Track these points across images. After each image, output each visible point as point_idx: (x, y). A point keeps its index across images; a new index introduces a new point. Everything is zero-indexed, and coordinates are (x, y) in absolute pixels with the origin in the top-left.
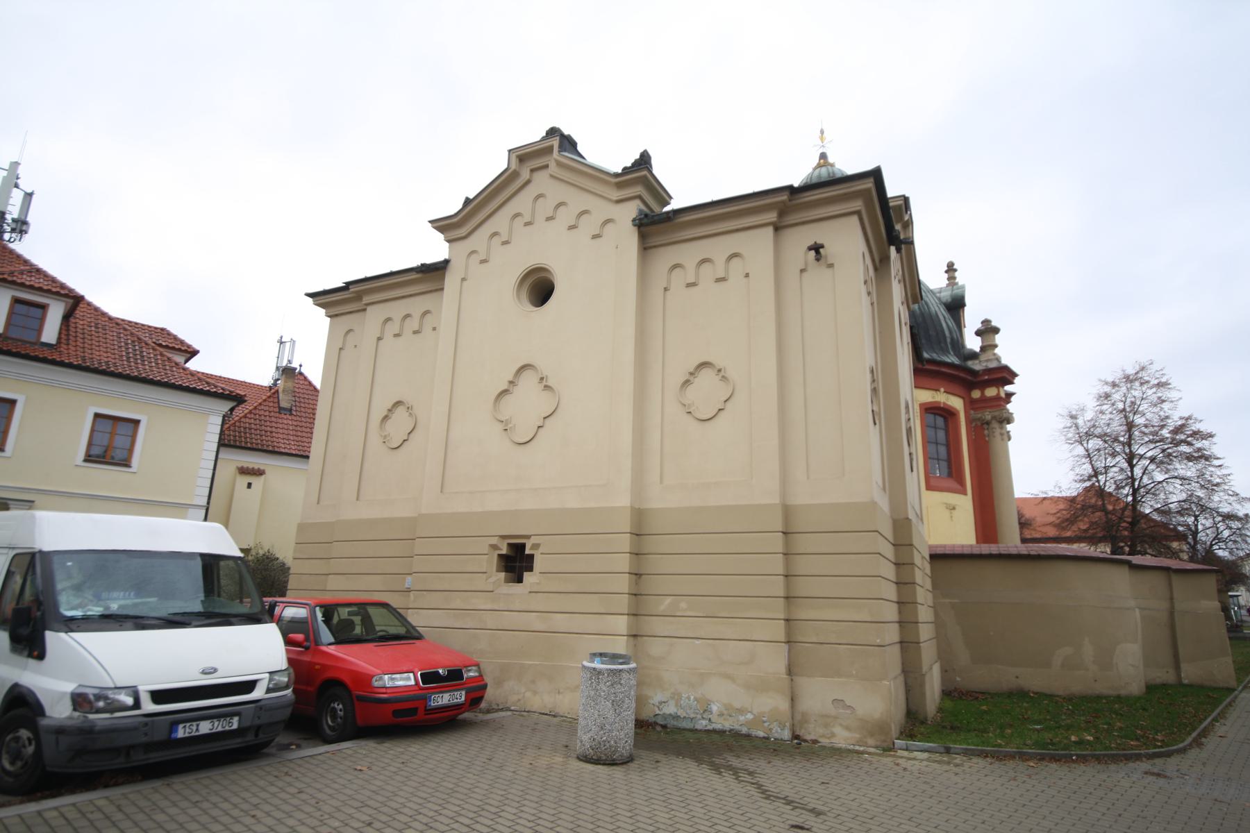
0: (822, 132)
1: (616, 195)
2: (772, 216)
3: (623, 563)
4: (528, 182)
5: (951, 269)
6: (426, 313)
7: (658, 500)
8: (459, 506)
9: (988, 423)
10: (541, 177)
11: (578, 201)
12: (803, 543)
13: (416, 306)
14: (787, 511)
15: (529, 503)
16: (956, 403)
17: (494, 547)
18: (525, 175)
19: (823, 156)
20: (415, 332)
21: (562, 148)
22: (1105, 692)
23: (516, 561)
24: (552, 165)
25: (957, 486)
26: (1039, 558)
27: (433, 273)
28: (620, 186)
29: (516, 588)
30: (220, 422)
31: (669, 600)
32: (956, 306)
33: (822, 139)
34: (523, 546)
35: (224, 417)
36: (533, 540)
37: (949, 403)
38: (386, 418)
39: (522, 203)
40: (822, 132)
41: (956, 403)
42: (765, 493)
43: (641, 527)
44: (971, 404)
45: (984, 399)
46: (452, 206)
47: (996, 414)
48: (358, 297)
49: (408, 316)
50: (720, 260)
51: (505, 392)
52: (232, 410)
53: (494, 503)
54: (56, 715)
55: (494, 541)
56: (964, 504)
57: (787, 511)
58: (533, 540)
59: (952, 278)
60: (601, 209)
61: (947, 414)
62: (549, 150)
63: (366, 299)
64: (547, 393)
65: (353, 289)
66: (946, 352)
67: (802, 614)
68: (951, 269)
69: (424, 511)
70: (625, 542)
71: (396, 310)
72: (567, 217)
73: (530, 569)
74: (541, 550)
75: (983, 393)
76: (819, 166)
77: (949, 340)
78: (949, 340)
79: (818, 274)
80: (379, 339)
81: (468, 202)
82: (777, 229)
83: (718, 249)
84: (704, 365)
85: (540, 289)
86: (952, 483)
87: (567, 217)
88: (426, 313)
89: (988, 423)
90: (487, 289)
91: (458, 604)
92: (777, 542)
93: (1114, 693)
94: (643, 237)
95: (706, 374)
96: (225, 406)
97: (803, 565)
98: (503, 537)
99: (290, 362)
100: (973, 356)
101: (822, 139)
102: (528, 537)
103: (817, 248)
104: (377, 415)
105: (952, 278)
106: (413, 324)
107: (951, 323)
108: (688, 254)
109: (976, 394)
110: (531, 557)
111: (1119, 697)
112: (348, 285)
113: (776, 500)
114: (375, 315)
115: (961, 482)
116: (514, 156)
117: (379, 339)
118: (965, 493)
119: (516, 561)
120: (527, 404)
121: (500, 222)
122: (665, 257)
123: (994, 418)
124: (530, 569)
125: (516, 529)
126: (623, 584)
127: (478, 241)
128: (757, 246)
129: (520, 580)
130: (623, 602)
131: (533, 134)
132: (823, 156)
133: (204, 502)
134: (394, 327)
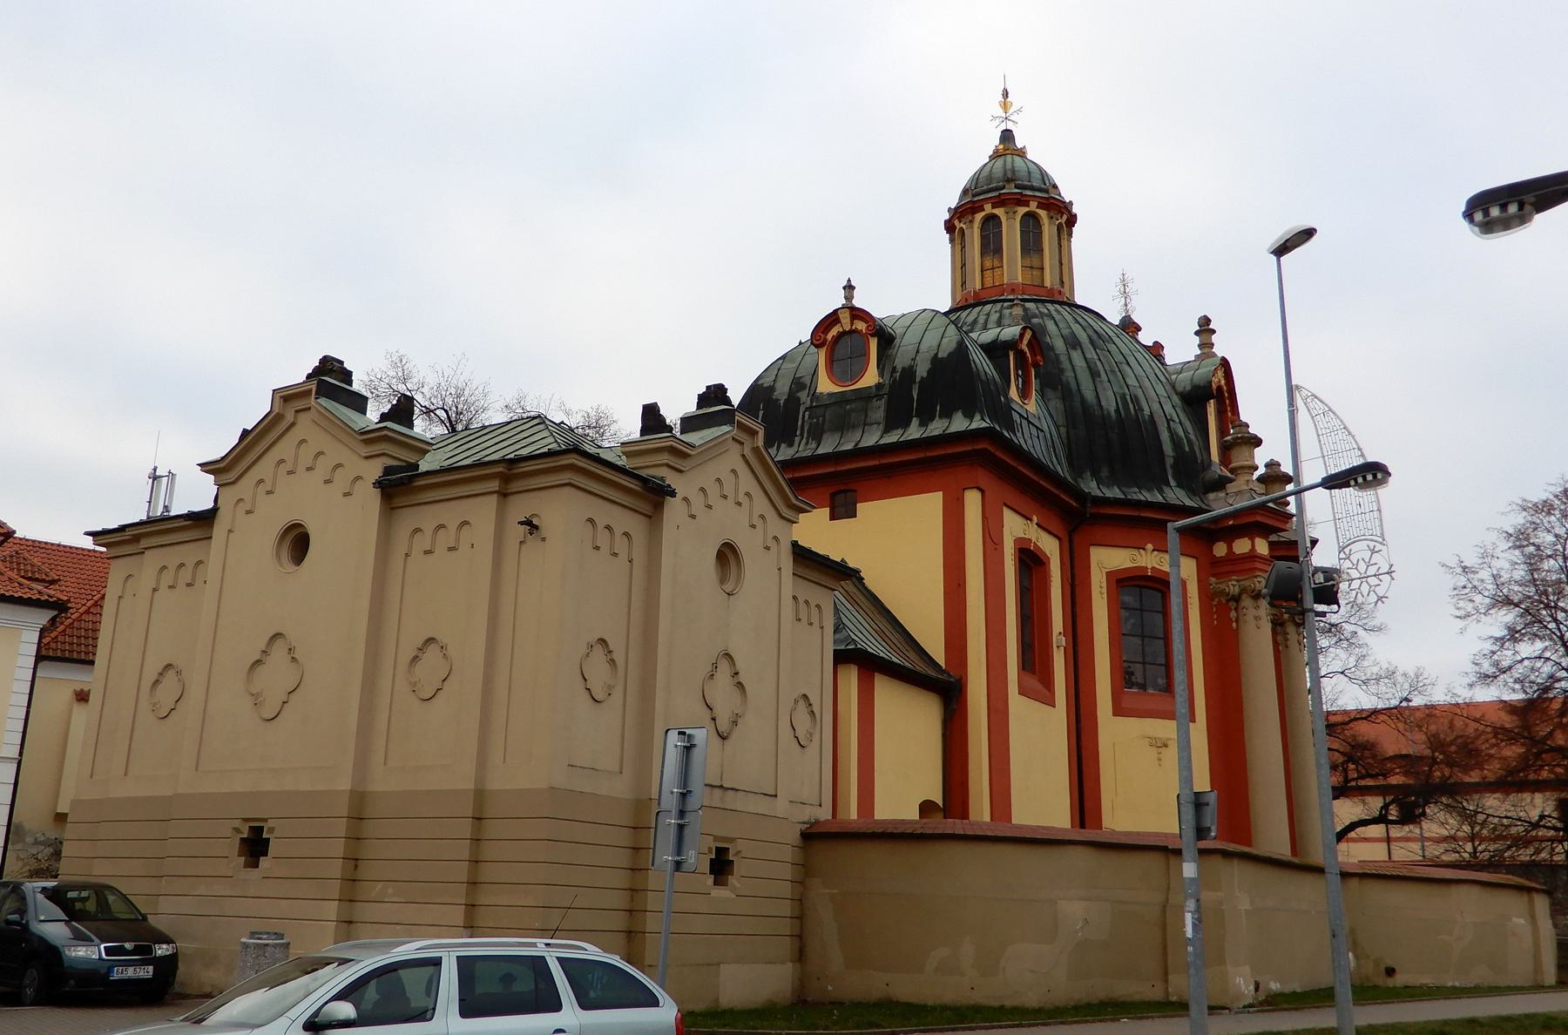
0: (1006, 94)
1: (366, 450)
4: (293, 425)
5: (1205, 329)
6: (200, 562)
7: (382, 782)
10: (303, 417)
12: (491, 829)
13: (189, 554)
17: (237, 830)
18: (290, 417)
19: (1007, 136)
20: (189, 585)
22: (985, 1002)
23: (255, 846)
27: (202, 520)
28: (367, 442)
29: (254, 874)
30: (35, 637)
31: (380, 885)
34: (262, 828)
35: (42, 631)
38: (157, 682)
39: (285, 449)
40: (1006, 94)
43: (359, 811)
44: (1211, 568)
45: (1232, 559)
46: (222, 444)
47: (1246, 583)
48: (136, 539)
49: (182, 565)
51: (258, 662)
52: (53, 620)
53: (241, 785)
55: (237, 824)
57: (480, 795)
58: (270, 824)
59: (1206, 345)
62: (307, 393)
63: (144, 543)
65: (129, 533)
66: (1160, 483)
67: (483, 899)
68: (1205, 329)
69: (180, 791)
70: (341, 828)
72: (324, 466)
74: (276, 834)
75: (1230, 548)
76: (996, 155)
77: (1169, 462)
78: (1169, 462)
80: (155, 590)
81: (245, 433)
82: (504, 495)
83: (451, 513)
84: (431, 640)
85: (297, 542)
87: (324, 466)
88: (200, 562)
90: (249, 543)
91: (202, 890)
92: (466, 828)
93: (996, 1004)
96: (43, 617)
97: (490, 851)
98: (246, 820)
99: (166, 508)
101: (1005, 106)
102: (265, 820)
103: (531, 525)
104: (150, 675)
105: (1206, 345)
106: (445, 538)
109: (1220, 550)
111: (1002, 1007)
112: (123, 528)
113: (345, 784)
114: (152, 560)
116: (277, 396)
117: (155, 590)
119: (255, 846)
121: (264, 469)
122: (409, 519)
123: (1243, 591)
126: (336, 869)
127: (245, 487)
128: (482, 512)
130: (335, 889)
131: (297, 372)
132: (1007, 136)
133: (14, 753)
134: (167, 578)
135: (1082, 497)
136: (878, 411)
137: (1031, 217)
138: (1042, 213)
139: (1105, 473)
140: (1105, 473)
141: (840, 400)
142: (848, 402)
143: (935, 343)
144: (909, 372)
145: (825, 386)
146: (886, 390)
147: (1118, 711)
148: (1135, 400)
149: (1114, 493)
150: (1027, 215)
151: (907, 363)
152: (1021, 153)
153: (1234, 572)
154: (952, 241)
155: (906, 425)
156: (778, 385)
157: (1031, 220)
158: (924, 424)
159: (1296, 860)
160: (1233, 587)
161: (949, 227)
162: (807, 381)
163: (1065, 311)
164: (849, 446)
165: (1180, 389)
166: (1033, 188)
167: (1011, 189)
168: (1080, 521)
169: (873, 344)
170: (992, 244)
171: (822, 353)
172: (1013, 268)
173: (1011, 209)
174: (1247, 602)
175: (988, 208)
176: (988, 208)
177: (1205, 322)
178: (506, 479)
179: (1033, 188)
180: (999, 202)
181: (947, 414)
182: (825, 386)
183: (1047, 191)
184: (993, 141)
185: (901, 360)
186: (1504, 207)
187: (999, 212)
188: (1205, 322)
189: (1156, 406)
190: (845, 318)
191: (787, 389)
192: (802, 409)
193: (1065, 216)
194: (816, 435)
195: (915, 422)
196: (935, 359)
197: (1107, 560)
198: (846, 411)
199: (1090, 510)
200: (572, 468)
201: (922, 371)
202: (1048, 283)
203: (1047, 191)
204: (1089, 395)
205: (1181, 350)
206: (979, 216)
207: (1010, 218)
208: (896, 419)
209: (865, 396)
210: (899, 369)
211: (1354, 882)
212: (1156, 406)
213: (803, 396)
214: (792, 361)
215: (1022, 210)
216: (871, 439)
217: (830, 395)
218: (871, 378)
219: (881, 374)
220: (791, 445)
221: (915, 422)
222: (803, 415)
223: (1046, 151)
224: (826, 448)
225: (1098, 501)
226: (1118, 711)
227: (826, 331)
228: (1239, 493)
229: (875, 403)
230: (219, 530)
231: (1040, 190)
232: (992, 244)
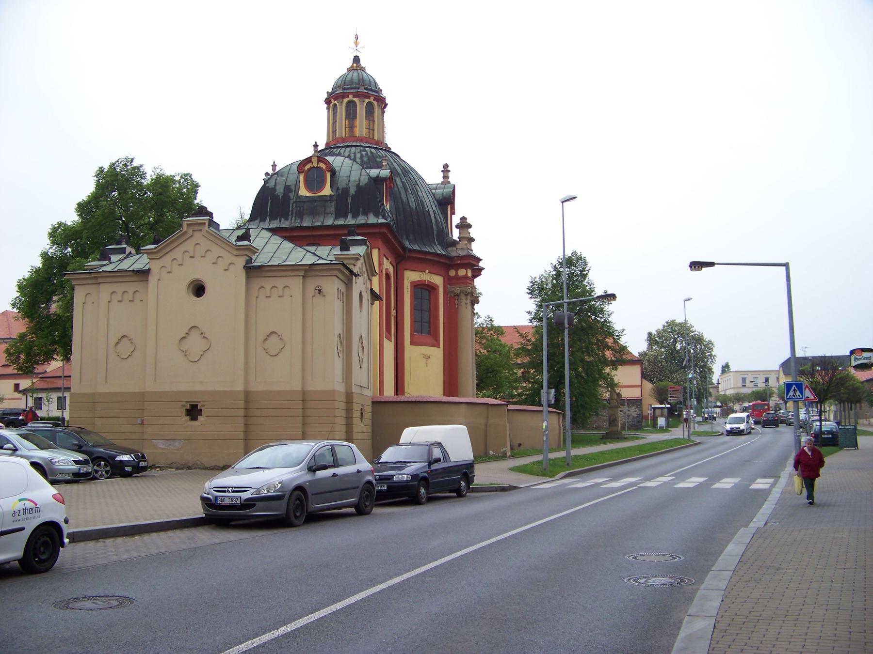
0: (357, 38)
1: (235, 253)
2: (302, 273)
3: (241, 412)
5: (446, 170)
8: (166, 388)
9: (458, 295)
10: (198, 235)
11: (217, 251)
13: (131, 287)
14: (304, 393)
15: (199, 388)
16: (437, 280)
18: (190, 233)
19: (356, 59)
21: (210, 225)
24: (204, 231)
25: (433, 341)
26: (400, 402)
29: (195, 423)
32: (447, 202)
33: (356, 44)
36: (202, 403)
37: (432, 281)
38: (117, 343)
40: (357, 38)
41: (437, 280)
42: (297, 386)
44: (448, 281)
45: (457, 277)
50: (280, 287)
51: (184, 338)
53: (183, 387)
54: (413, 394)
55: (184, 403)
56: (437, 354)
58: (202, 403)
59: (446, 177)
60: (229, 258)
61: (431, 288)
63: (100, 280)
64: (204, 340)
66: (431, 243)
68: (446, 170)
69: (147, 390)
70: (242, 405)
71: (119, 288)
73: (201, 415)
75: (457, 273)
76: (351, 69)
77: (435, 232)
78: (435, 232)
79: (318, 298)
83: (280, 282)
85: (199, 290)
86: (430, 339)
87: (211, 257)
89: (458, 295)
94: (247, 273)
95: (274, 336)
100: (454, 243)
101: (356, 44)
104: (113, 340)
105: (446, 177)
107: (440, 218)
108: (268, 283)
109: (452, 273)
110: (201, 410)
113: (300, 389)
115: (437, 339)
118: (438, 346)
119: (194, 412)
120: (195, 344)
122: (257, 283)
123: (462, 292)
124: (201, 415)
125: (194, 399)
128: (296, 284)
129: (196, 419)
132: (356, 59)
134: (118, 297)
135: (404, 248)
136: (332, 208)
137: (370, 104)
138: (375, 103)
139: (411, 237)
140: (411, 237)
141: (311, 200)
142: (315, 201)
143: (357, 178)
144: (346, 190)
145: (303, 192)
146: (335, 198)
147: (413, 343)
148: (422, 202)
149: (416, 247)
150: (368, 103)
151: (344, 186)
152: (363, 69)
153: (457, 284)
154: (328, 108)
155: (346, 217)
156: (278, 188)
157: (370, 106)
158: (355, 216)
159: (400, 398)
160: (457, 290)
161: (328, 101)
162: (293, 187)
163: (387, 154)
164: (319, 224)
165: (437, 197)
166: (372, 90)
167: (362, 90)
168: (402, 259)
169: (328, 175)
170: (351, 114)
171: (302, 177)
172: (361, 128)
173: (356, 98)
174: (462, 297)
175: (351, 97)
176: (351, 97)
177: (446, 166)
178: (306, 271)
179: (372, 90)
180: (356, 95)
181: (366, 213)
182: (303, 192)
183: (377, 92)
184: (349, 63)
185: (342, 184)
186: (696, 266)
187: (356, 100)
188: (446, 166)
189: (429, 206)
190: (315, 160)
191: (282, 191)
192: (291, 202)
193: (382, 102)
194: (300, 215)
195: (350, 215)
196: (358, 186)
197: (411, 276)
198: (315, 206)
199: (407, 254)
200: (340, 270)
201: (352, 191)
202: (376, 138)
203: (377, 92)
204: (404, 199)
205: (431, 176)
206: (346, 100)
207: (362, 102)
208: (340, 213)
209: (324, 199)
210: (341, 188)
211: (511, 412)
212: (429, 206)
213: (292, 195)
214: (282, 176)
215: (367, 101)
216: (329, 222)
217: (307, 197)
218: (327, 191)
219: (332, 190)
220: (287, 219)
221: (350, 215)
222: (292, 206)
223: (373, 69)
224: (306, 223)
225: (411, 251)
226: (413, 343)
227: (304, 166)
228: (462, 249)
229: (329, 203)
230: (152, 279)
231: (375, 91)
232: (351, 114)
